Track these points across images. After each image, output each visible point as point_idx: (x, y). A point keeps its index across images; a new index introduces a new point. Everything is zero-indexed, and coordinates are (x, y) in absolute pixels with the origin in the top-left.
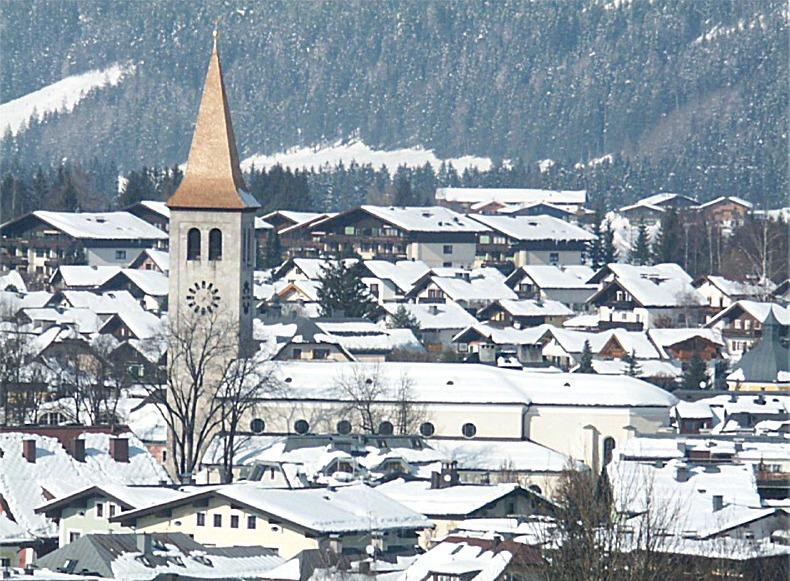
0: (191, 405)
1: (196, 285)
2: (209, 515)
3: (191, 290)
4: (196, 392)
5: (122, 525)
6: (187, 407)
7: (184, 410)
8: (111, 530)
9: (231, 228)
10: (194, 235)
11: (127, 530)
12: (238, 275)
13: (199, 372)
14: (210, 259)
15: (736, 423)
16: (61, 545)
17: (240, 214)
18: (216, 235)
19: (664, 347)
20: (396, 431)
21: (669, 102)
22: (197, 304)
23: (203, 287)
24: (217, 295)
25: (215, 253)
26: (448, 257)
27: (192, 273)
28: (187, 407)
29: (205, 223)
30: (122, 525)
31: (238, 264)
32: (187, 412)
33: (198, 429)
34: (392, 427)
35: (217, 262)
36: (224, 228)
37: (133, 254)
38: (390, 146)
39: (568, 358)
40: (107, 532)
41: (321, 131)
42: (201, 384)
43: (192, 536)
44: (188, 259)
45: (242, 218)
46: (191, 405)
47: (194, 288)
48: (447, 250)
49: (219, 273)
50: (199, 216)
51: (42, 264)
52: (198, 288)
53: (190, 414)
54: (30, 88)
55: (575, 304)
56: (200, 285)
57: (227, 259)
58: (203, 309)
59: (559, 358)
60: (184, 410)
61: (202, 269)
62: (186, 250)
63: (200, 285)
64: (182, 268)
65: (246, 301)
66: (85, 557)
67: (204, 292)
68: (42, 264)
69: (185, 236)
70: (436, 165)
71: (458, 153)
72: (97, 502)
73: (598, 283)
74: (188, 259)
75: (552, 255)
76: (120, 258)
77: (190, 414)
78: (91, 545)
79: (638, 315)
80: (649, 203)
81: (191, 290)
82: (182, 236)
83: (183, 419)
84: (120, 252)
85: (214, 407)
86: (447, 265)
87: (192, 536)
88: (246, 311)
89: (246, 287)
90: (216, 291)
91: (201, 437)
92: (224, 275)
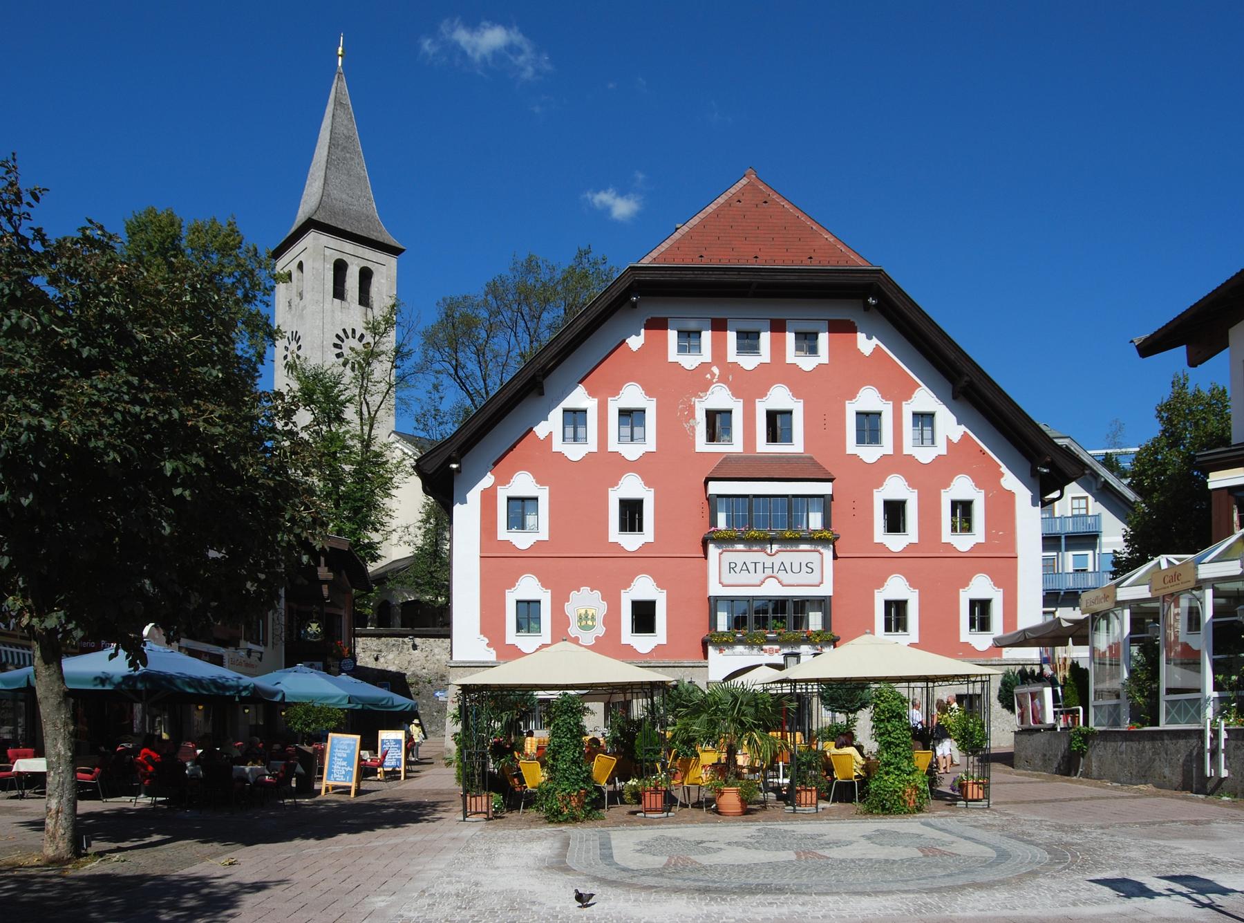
1: (344, 330)
3: (338, 336)
27: (338, 315)
47: (342, 334)
50: (349, 247)
56: (349, 333)
63: (349, 333)
74: (334, 297)
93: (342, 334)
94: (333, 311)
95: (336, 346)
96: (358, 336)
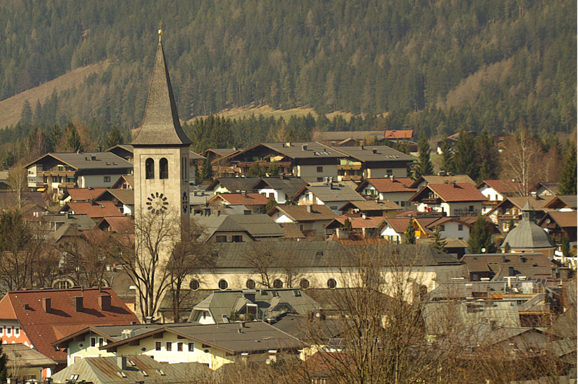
0: (151, 273)
2: (163, 342)
3: (149, 199)
4: (154, 264)
5: (107, 352)
6: (148, 275)
7: (146, 277)
8: (100, 355)
9: (174, 157)
10: (150, 163)
11: (111, 354)
12: (179, 188)
13: (156, 250)
14: (160, 178)
15: (392, 230)
16: (69, 365)
17: (178, 151)
18: (164, 163)
19: (507, 243)
20: (284, 286)
21: (469, 68)
22: (152, 205)
23: (154, 198)
24: (166, 201)
25: (164, 175)
26: (320, 174)
28: (148, 275)
29: (156, 155)
30: (107, 352)
31: (179, 181)
32: (148, 278)
33: (155, 290)
34: (282, 283)
35: (165, 180)
36: (169, 157)
37: (114, 179)
38: (285, 108)
39: (398, 237)
40: (98, 356)
41: (250, 98)
42: (157, 259)
43: (152, 357)
44: (147, 178)
45: (181, 151)
46: (151, 273)
47: (151, 197)
48: (320, 170)
49: (166, 187)
50: (152, 151)
51: (57, 187)
52: (154, 198)
53: (150, 279)
54: (52, 77)
55: (402, 202)
57: (172, 178)
58: (154, 210)
59: (392, 236)
60: (146, 277)
61: (156, 185)
62: (145, 173)
64: (143, 184)
65: (185, 201)
66: (84, 373)
67: (157, 200)
68: (57, 187)
69: (143, 164)
70: (315, 116)
71: (332, 108)
72: (91, 338)
73: (417, 188)
74: (147, 178)
75: (388, 171)
76: (107, 181)
77: (150, 279)
78: (88, 365)
79: (443, 208)
80: (453, 137)
81: (149, 199)
82: (142, 164)
83: (146, 282)
84: (107, 177)
85: (167, 274)
86: (320, 179)
87: (152, 357)
88: (185, 210)
89: (185, 196)
90: (157, 194)
91: (158, 293)
92: (170, 188)
93: (151, 197)
94: (146, 186)
95: (147, 203)
96: (159, 195)
